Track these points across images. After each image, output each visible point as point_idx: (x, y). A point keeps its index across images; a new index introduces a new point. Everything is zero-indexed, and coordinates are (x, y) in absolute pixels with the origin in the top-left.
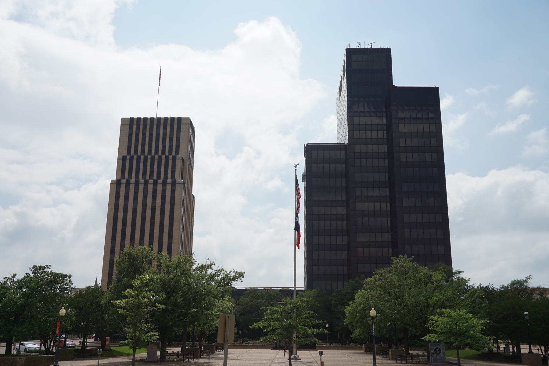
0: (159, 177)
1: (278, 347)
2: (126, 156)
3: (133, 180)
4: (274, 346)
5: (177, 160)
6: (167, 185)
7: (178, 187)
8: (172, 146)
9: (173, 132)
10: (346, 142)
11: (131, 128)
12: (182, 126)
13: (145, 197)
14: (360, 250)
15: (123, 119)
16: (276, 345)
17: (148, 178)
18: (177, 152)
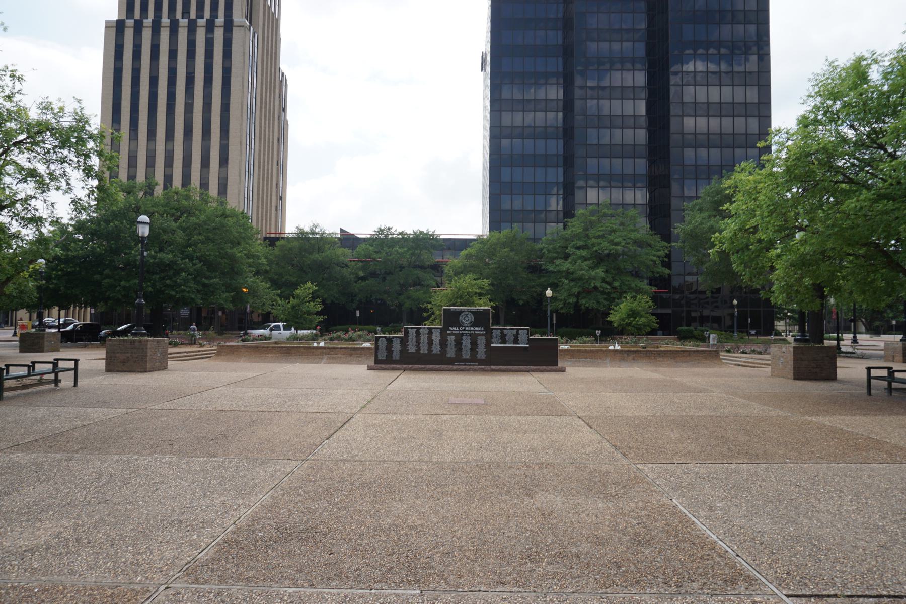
0: (200, 15)
1: (396, 356)
3: (220, 20)
4: (382, 355)
6: (216, 29)
7: (236, 34)
13: (173, 54)
14: (689, 153)
16: (389, 350)
17: (179, 15)
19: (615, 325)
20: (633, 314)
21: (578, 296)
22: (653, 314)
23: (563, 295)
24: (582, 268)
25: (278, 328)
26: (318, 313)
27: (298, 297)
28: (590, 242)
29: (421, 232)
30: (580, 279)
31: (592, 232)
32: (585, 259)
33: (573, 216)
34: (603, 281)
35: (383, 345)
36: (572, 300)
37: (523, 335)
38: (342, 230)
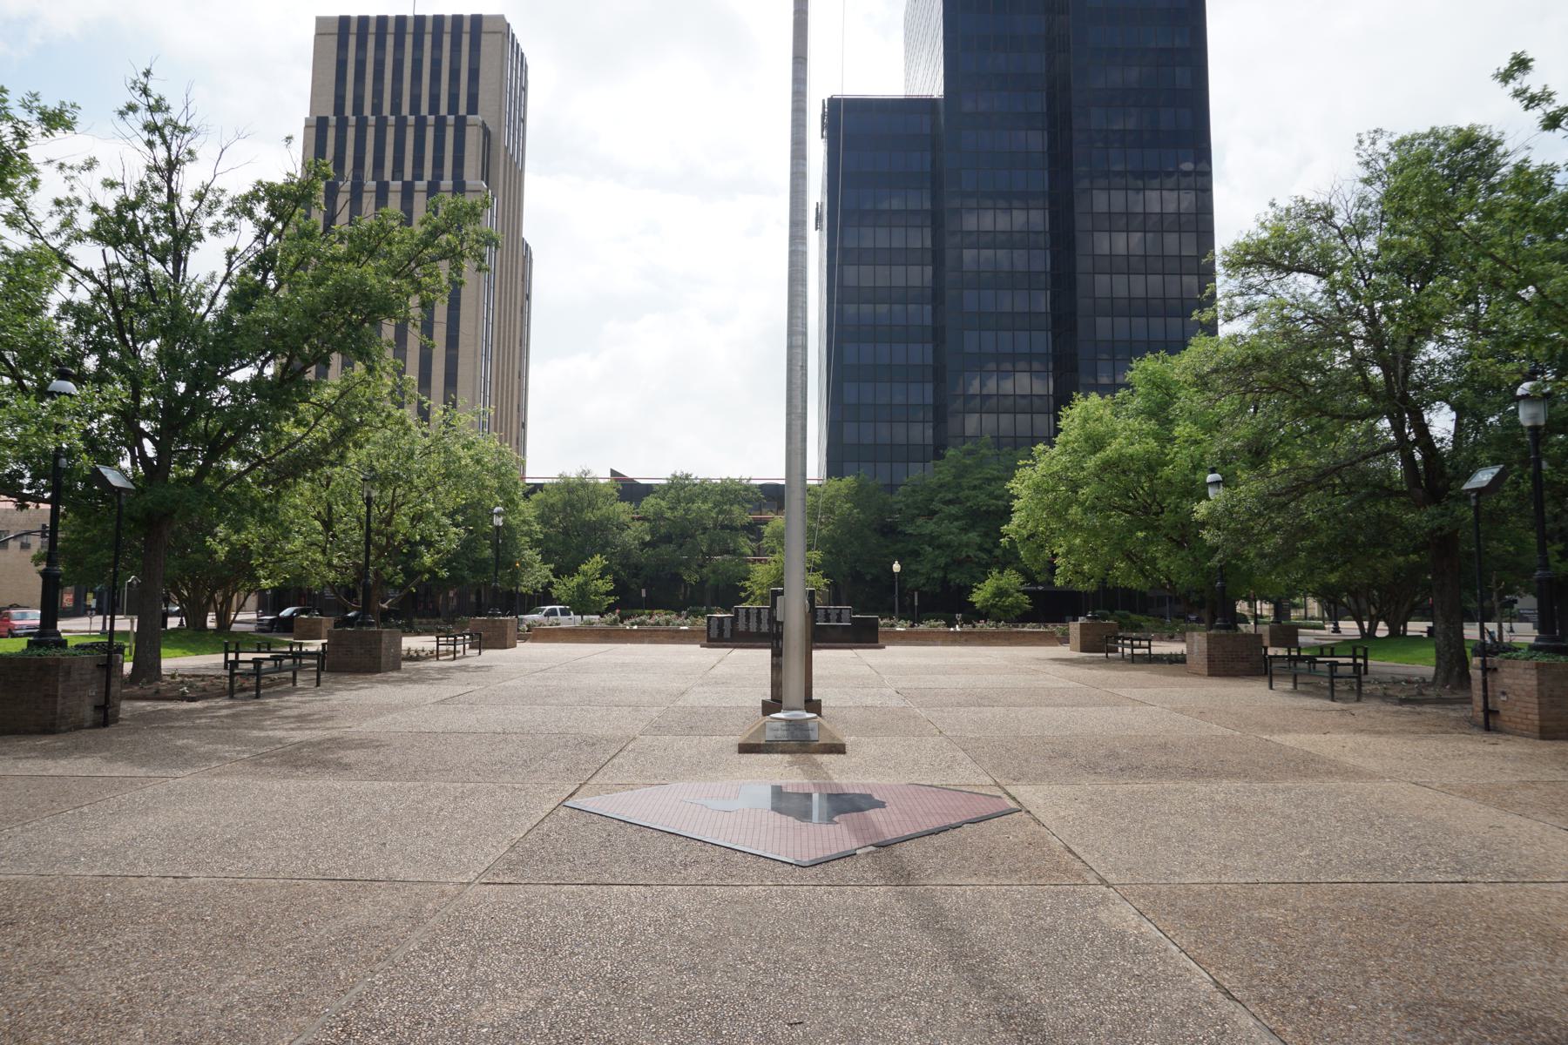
0: (418, 176)
1: (727, 634)
2: (469, 112)
4: (714, 633)
5: (468, 130)
8: (419, 96)
9: (460, 51)
10: (930, 83)
11: (342, 45)
12: (484, 37)
15: (321, 22)
17: (388, 176)
18: (473, 108)
19: (978, 605)
20: (1001, 593)
21: (946, 568)
22: (1025, 592)
23: (924, 568)
24: (949, 531)
25: (553, 612)
26: (608, 594)
27: (585, 574)
28: (962, 494)
29: (732, 481)
30: (948, 545)
31: (964, 482)
32: (957, 518)
33: (942, 457)
34: (981, 548)
35: (714, 625)
36: (937, 574)
37: (845, 615)
38: (613, 473)
